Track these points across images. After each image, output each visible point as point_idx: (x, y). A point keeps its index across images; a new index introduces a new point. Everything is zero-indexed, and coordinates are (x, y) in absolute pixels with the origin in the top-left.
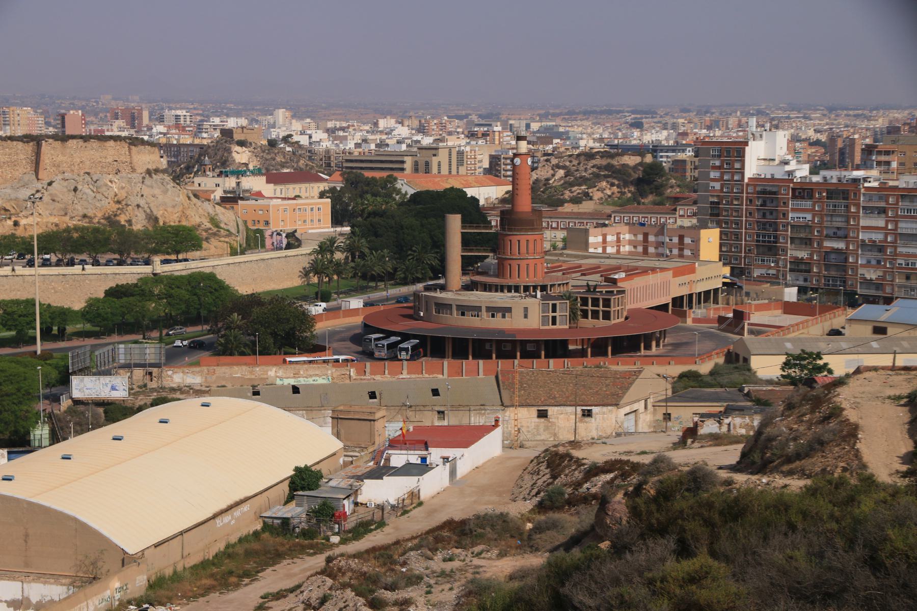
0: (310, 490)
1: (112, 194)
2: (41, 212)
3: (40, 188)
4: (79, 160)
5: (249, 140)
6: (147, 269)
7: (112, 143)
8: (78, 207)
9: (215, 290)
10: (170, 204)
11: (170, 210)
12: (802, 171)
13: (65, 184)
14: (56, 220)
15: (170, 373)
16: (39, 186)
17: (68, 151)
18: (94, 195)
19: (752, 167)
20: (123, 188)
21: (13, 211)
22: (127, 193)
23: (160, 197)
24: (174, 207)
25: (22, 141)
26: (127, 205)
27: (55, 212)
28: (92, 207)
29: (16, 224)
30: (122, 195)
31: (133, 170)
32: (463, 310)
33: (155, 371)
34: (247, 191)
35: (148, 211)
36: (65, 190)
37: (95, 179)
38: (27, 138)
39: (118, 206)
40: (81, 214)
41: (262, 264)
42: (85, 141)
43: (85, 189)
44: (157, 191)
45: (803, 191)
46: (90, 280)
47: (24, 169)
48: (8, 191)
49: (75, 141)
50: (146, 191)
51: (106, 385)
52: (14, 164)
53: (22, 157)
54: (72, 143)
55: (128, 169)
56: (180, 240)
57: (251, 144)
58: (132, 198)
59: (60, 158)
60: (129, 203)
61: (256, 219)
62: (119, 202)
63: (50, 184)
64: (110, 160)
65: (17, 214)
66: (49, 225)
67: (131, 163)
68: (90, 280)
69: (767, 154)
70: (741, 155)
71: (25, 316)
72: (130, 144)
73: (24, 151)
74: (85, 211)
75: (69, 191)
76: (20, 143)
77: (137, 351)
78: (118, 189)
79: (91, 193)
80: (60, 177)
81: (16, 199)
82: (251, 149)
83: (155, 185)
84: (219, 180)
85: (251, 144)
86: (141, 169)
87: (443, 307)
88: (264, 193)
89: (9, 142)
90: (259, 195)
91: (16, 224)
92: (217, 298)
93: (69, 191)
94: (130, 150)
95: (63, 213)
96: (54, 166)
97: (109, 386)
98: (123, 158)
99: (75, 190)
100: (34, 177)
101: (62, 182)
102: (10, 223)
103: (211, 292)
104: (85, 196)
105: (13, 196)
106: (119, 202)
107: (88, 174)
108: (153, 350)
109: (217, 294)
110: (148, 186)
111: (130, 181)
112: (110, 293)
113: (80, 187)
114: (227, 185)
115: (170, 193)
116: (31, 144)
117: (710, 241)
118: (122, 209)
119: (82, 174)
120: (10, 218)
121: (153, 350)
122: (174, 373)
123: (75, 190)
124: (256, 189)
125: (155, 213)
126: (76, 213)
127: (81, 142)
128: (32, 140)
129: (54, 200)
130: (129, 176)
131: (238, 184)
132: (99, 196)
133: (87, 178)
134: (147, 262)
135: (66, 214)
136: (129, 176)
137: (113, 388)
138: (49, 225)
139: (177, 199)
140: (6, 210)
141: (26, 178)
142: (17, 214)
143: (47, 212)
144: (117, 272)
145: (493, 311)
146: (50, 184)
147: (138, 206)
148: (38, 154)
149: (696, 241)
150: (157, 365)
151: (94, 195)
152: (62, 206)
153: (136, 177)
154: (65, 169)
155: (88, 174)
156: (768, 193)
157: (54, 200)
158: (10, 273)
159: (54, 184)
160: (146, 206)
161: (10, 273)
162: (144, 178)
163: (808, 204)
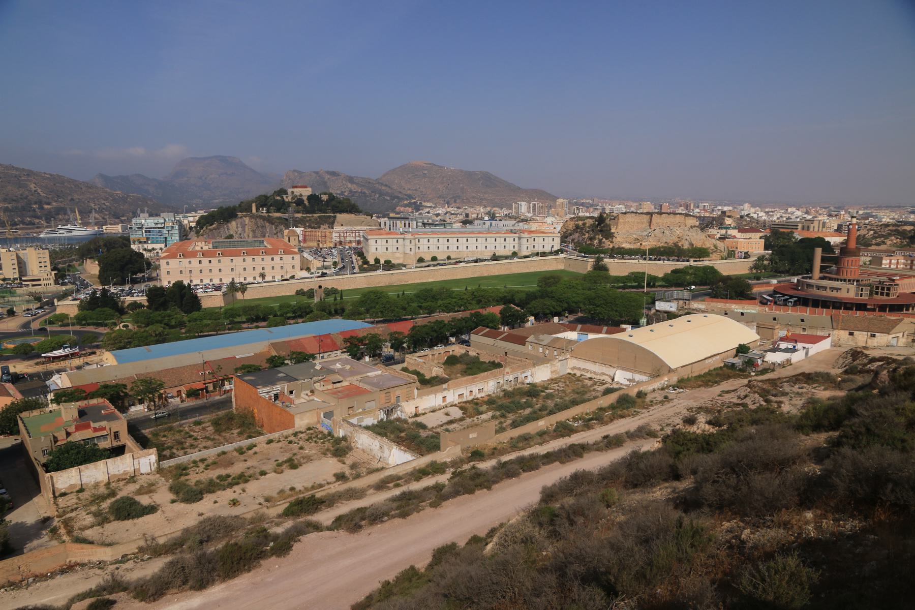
6: (688, 263)
10: (699, 239)
28: (669, 239)
32: (819, 288)
38: (647, 213)
43: (667, 232)
47: (646, 224)
50: (690, 234)
52: (642, 223)
56: (701, 253)
90: (734, 237)
108: (381, 242)
121: (381, 242)
134: (688, 261)
145: (832, 289)
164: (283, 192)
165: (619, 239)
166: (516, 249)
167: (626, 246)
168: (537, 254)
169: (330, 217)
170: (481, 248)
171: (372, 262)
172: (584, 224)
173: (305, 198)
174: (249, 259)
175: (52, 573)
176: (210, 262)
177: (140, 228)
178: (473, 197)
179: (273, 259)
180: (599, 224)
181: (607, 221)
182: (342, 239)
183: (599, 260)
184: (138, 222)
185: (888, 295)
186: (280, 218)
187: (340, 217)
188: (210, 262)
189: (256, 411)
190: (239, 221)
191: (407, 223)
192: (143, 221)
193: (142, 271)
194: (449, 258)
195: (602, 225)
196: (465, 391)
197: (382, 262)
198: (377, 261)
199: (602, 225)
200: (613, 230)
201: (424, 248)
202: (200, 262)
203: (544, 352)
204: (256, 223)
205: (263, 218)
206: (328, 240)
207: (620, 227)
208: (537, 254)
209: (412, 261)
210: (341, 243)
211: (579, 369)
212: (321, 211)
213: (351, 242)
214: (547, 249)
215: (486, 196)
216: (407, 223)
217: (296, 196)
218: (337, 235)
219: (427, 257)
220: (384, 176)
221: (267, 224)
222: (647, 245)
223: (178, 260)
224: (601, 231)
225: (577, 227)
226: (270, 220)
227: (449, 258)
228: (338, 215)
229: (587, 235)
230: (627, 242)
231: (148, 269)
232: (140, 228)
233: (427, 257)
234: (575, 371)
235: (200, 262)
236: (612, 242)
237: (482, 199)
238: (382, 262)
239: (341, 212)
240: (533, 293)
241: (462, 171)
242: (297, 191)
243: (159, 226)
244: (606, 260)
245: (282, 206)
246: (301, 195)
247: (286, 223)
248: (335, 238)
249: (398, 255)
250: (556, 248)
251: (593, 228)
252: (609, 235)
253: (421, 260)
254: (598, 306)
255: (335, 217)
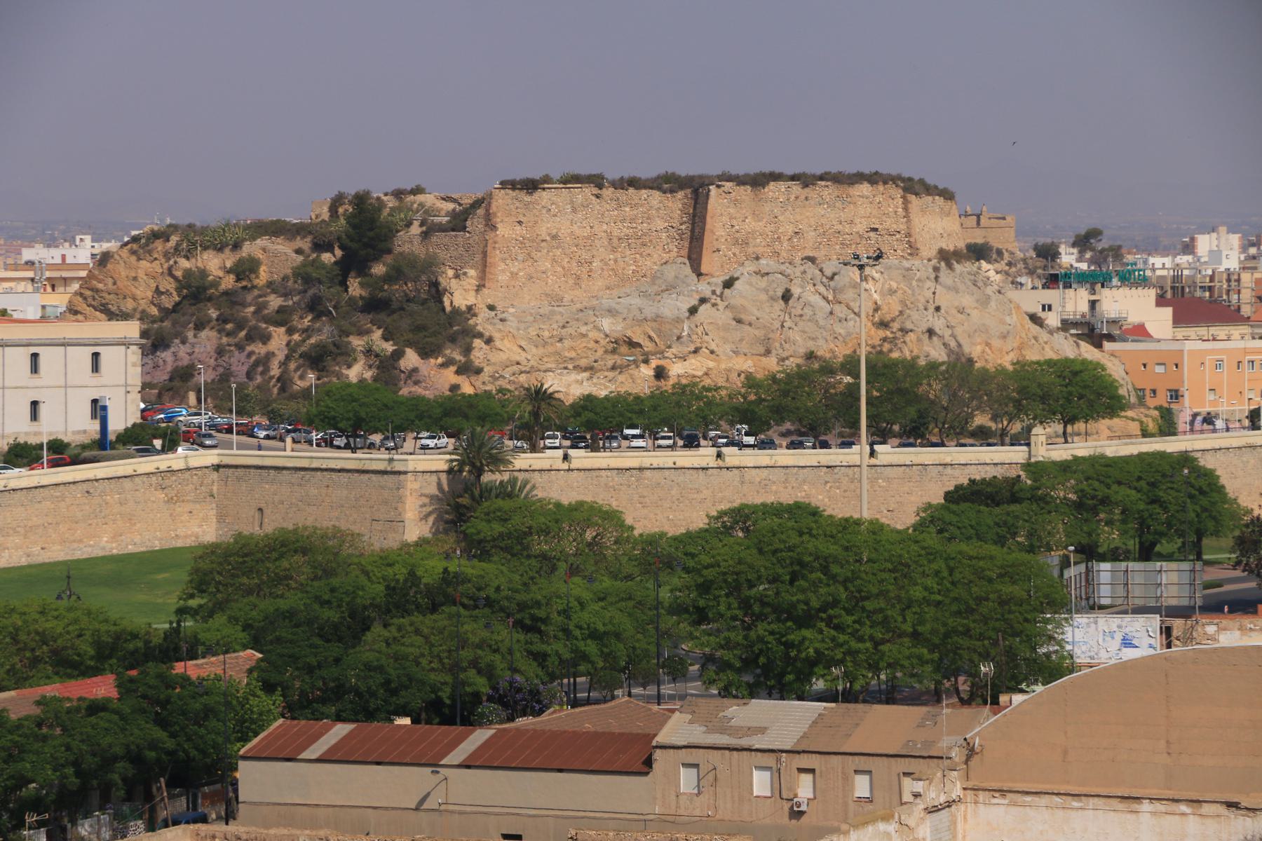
1: (866, 307)
2: (713, 346)
3: (708, 294)
4: (791, 229)
5: (996, 244)
6: (1017, 454)
7: (865, 188)
8: (795, 336)
9: (1201, 492)
11: (996, 343)
13: (763, 283)
14: (747, 365)
15: (1211, 629)
16: (704, 288)
17: (767, 208)
18: (828, 308)
20: (892, 292)
21: (648, 346)
22: (903, 302)
23: (974, 313)
24: (1004, 337)
25: (659, 189)
26: (905, 331)
27: (744, 347)
28: (837, 329)
29: (660, 373)
30: (891, 307)
31: (913, 250)
33: (1178, 624)
34: (1114, 322)
35: (953, 344)
36: (764, 297)
37: (828, 272)
38: (668, 183)
39: (882, 333)
40: (802, 351)
41: (1248, 456)
42: (806, 186)
43: (807, 294)
44: (967, 300)
46: (888, 480)
47: (665, 253)
48: (636, 301)
49: (782, 186)
50: (944, 299)
51: (1112, 634)
52: (640, 242)
53: (660, 224)
54: (773, 189)
55: (901, 248)
56: (1076, 394)
57: (1000, 253)
58: (915, 316)
59: (751, 224)
60: (909, 325)
61: (1148, 387)
62: (884, 324)
63: (729, 284)
64: (861, 227)
65: (661, 353)
66: (734, 376)
67: (909, 235)
68: (888, 480)
71: (712, 566)
72: (906, 190)
73: (666, 210)
74: (811, 345)
75: (773, 299)
76: (657, 193)
77: (1138, 579)
78: (882, 294)
79: (823, 303)
80: (750, 267)
81: (657, 318)
82: (1002, 265)
83: (961, 287)
84: (1051, 296)
85: (1000, 253)
86: (929, 250)
88: (1150, 328)
89: (631, 190)
90: (1140, 332)
91: (660, 373)
92: (1205, 510)
93: (773, 299)
94: (906, 203)
95: (762, 350)
96: (736, 242)
97: (1119, 637)
98: (890, 224)
99: (786, 297)
100: (687, 270)
101: (755, 279)
102: (647, 371)
103: (1191, 497)
104: (808, 311)
105: (649, 311)
106: (884, 324)
107: (812, 260)
109: (1204, 501)
110: (949, 288)
111: (907, 274)
112: (956, 496)
113: (796, 291)
114: (1070, 307)
115: (993, 304)
116: (680, 194)
118: (893, 341)
119: (798, 260)
120: (646, 362)
121: (1174, 577)
122: (1220, 630)
123: (786, 297)
124: (1133, 319)
125: (966, 349)
126: (789, 349)
127: (796, 188)
128: (681, 188)
129: (739, 321)
130: (906, 264)
131: (1093, 304)
132: (840, 310)
133: (812, 270)
134: (1023, 439)
135: (768, 352)
136: (906, 264)
137: (1127, 643)
138: (734, 376)
139: (1008, 319)
140: (632, 344)
141: (670, 273)
142: (661, 353)
143: (728, 347)
144: (948, 460)
146: (729, 284)
147: (931, 332)
150: (1184, 612)
151: (828, 308)
152: (760, 333)
153: (922, 267)
154: (760, 250)
155: (812, 260)
157: (739, 321)
158: (712, 462)
159: (737, 284)
160: (947, 333)
161: (712, 462)
162: (936, 269)
167: (569, 386)
172: (245, 270)
175: (1222, 611)
180: (353, 263)
181: (409, 241)
183: (476, 459)
189: (606, 324)
195: (371, 265)
199: (371, 265)
200: (460, 295)
203: (779, 791)
207: (502, 271)
214: (77, 425)
224: (375, 306)
229: (279, 340)
230: (565, 364)
236: (467, 369)
240: (637, 398)
244: (524, 461)
250: (118, 423)
251: (310, 294)
252: (447, 331)
254: (806, 620)
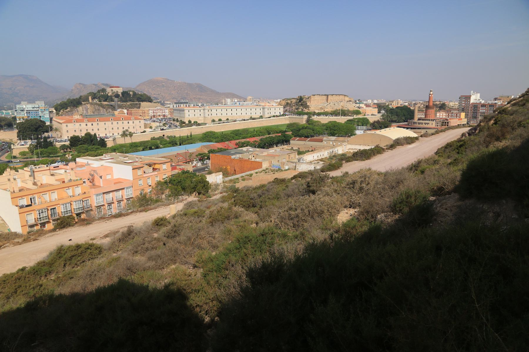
0: (448, 146)
10: (352, 107)
12: (483, 102)
19: (472, 101)
28: (338, 107)
32: (419, 123)
38: (325, 95)
45: (483, 105)
56: (358, 113)
69: (475, 98)
70: (470, 98)
73: (325, 97)
87: (414, 123)
108: (192, 112)
117: (463, 115)
121: (192, 112)
145: (425, 124)
148: (327, 98)
149: (460, 115)
156: (475, 106)
163: (485, 108)
164: (104, 90)
165: (312, 108)
166: (261, 114)
167: (317, 111)
168: (274, 116)
169: (137, 104)
170: (244, 114)
171: (187, 122)
172: (291, 102)
173: (120, 94)
174: (115, 123)
176: (92, 125)
177: (22, 110)
178: (194, 98)
179: (128, 123)
180: (300, 101)
181: (304, 100)
182: (155, 114)
183: (309, 117)
184: (21, 107)
185: (448, 125)
186: (107, 105)
187: (143, 104)
188: (92, 125)
190: (84, 106)
191: (188, 105)
192: (24, 106)
193: (47, 132)
194: (228, 119)
195: (301, 101)
196: (318, 154)
197: (193, 122)
198: (190, 122)
200: (308, 104)
201: (214, 115)
202: (86, 125)
204: (95, 108)
205: (96, 104)
206: (146, 114)
207: (312, 102)
208: (274, 116)
209: (209, 121)
210: (154, 116)
211: (352, 149)
212: (131, 101)
213: (159, 116)
215: (202, 97)
216: (188, 105)
217: (114, 92)
218: (152, 112)
219: (217, 119)
220: (138, 86)
221: (101, 108)
222: (329, 109)
223: (73, 124)
224: (302, 105)
225: (287, 103)
226: (103, 106)
227: (228, 119)
228: (141, 103)
231: (51, 131)
232: (22, 110)
233: (217, 119)
234: (350, 150)
235: (86, 125)
237: (199, 99)
238: (193, 122)
239: (143, 101)
241: (185, 83)
242: (115, 90)
243: (35, 109)
245: (107, 98)
246: (117, 92)
247: (114, 108)
248: (151, 114)
249: (200, 118)
251: (297, 104)
252: (307, 107)
253: (213, 121)
255: (140, 104)
